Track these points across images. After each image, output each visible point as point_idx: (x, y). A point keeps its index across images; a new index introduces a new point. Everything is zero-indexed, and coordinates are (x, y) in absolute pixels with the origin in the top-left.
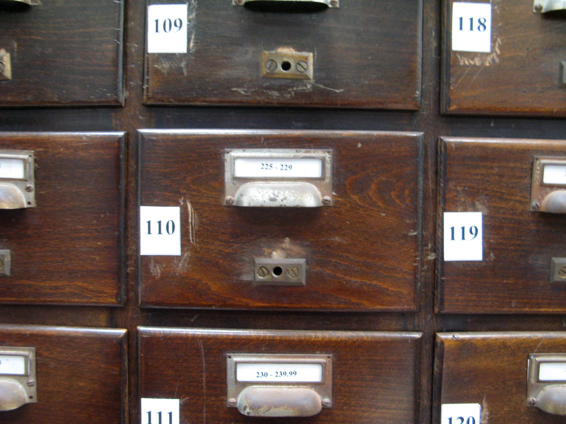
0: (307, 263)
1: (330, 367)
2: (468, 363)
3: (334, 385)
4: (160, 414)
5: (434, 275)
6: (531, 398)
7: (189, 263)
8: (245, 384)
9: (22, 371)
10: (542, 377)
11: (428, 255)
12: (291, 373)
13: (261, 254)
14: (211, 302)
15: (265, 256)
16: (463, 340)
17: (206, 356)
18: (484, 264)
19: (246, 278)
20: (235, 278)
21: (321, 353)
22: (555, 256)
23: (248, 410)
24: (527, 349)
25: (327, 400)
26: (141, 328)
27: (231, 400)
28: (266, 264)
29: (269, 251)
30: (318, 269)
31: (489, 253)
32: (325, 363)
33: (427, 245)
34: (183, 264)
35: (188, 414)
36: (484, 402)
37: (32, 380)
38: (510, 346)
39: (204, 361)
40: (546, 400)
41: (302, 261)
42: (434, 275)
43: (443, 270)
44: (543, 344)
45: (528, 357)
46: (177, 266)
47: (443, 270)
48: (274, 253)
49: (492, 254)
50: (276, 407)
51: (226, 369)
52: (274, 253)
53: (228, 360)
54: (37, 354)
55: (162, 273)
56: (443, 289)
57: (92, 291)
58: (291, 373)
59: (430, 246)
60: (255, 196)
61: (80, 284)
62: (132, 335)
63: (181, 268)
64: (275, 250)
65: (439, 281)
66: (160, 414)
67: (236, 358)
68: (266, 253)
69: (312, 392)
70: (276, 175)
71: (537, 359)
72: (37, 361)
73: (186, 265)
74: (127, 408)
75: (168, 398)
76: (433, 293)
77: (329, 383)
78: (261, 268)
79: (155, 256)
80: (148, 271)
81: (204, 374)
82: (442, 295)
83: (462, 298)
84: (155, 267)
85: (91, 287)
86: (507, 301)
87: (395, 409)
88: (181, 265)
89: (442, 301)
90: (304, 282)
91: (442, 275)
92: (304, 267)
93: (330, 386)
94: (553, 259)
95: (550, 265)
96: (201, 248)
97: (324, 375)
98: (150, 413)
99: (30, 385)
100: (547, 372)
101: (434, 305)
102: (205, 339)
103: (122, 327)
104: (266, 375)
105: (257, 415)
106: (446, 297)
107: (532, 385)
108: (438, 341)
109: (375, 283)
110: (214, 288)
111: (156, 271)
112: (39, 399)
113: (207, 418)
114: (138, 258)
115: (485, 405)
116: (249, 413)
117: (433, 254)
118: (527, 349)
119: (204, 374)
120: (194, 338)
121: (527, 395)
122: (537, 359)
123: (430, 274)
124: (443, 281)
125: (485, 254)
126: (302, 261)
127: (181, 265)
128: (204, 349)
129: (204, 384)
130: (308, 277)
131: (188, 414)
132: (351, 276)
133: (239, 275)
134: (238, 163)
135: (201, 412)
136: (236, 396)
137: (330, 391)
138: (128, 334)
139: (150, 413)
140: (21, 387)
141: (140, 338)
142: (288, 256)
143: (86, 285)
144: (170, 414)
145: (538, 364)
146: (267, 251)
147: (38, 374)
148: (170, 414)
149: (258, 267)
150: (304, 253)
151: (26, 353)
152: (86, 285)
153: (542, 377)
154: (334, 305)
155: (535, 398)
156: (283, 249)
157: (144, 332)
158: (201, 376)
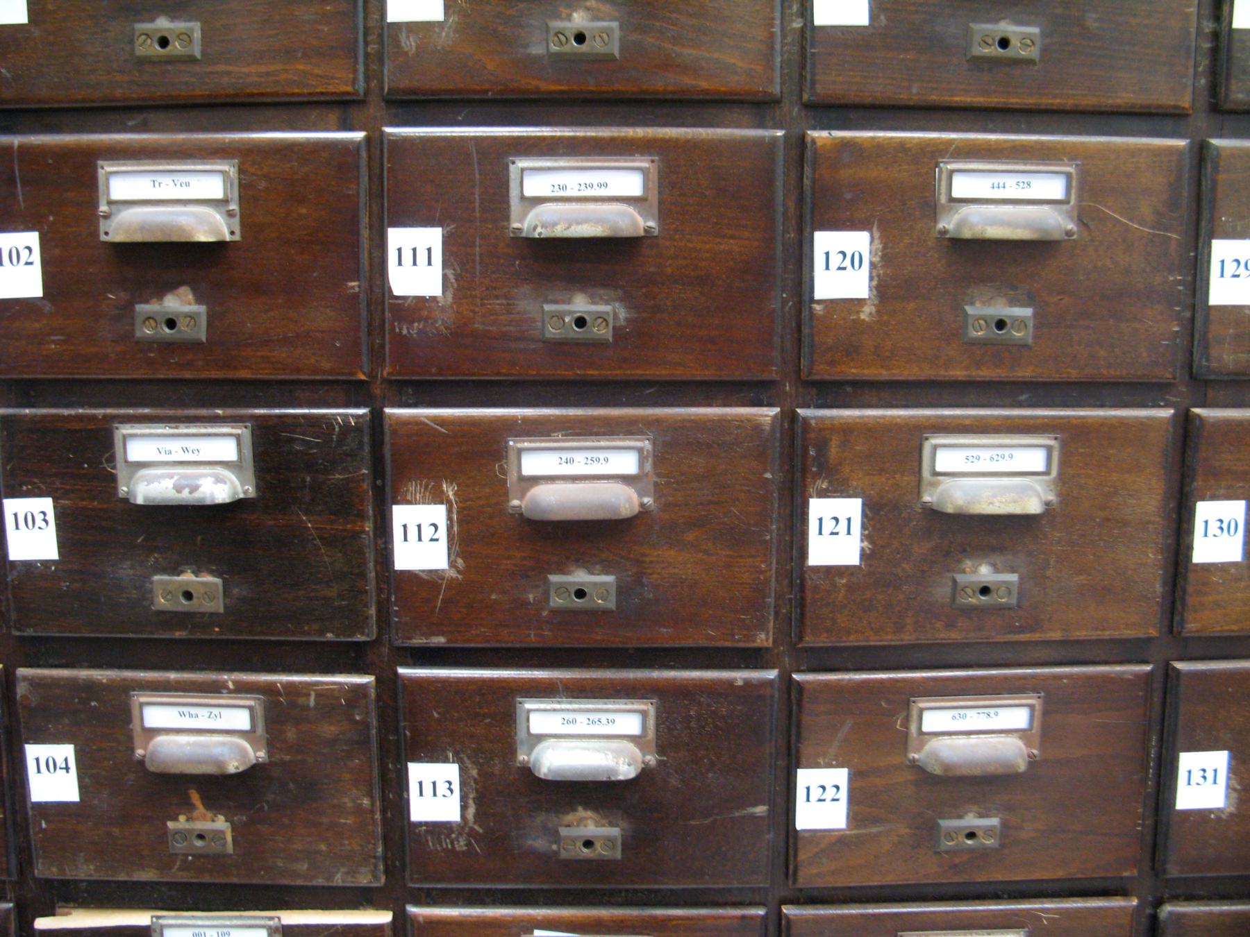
0: (621, 27)
1: (654, 175)
2: (851, 172)
3: (661, 202)
4: (414, 250)
5: (803, 48)
6: (941, 225)
7: (456, 31)
8: (535, 480)
9: (219, 195)
10: (956, 193)
11: (792, 21)
12: (600, 185)
13: (558, 16)
14: (486, 86)
15: (562, 19)
16: (843, 139)
17: (479, 164)
18: (872, 31)
19: (537, 50)
20: (521, 50)
21: (642, 155)
22: (974, 21)
23: (539, 230)
24: (920, 431)
25: (651, 224)
26: (388, 130)
27: (522, 757)
28: (565, 28)
29: (568, 11)
30: (635, 37)
31: (878, 16)
32: (648, 169)
33: (790, 7)
34: (448, 33)
35: (455, 249)
36: (875, 229)
37: (234, 206)
38: (910, 149)
39: (477, 172)
40: (935, 756)
41: (615, 25)
42: (803, 48)
43: (813, 37)
44: (957, 148)
45: (937, 165)
46: (439, 37)
47: (813, 37)
48: (575, 15)
49: (882, 17)
50: (578, 223)
51: (508, 181)
52: (575, 15)
53: (512, 167)
54: (241, 171)
55: (418, 47)
56: (814, 65)
57: (318, 76)
58: (600, 185)
59: (795, 8)
60: (551, 499)
61: (301, 67)
62: (375, 142)
63: (444, 39)
64: (575, 10)
65: (808, 55)
66: (414, 250)
67: (523, 163)
68: (564, 15)
69: (630, 210)
70: (581, 191)
71: (949, 167)
72: (240, 180)
73: (452, 35)
74: (366, 246)
75: (425, 226)
76: (801, 75)
77: (654, 198)
78: (556, 34)
79: (407, 23)
80: (397, 44)
81: (477, 191)
82: (813, 74)
83: (840, 79)
84: (408, 37)
85: (316, 71)
86: (907, 84)
87: (748, 239)
88: (444, 34)
89: (813, 83)
90: (617, 54)
91: (812, 46)
92: (617, 34)
93: (656, 203)
94: (971, 25)
95: (968, 33)
96: (472, 10)
97: (641, 464)
98: (400, 250)
99: (230, 214)
100: (963, 186)
101: (801, 91)
102: (478, 140)
103: (361, 129)
104: (564, 188)
105: (552, 235)
106: (818, 78)
107: (943, 206)
108: (808, 139)
109: (716, 55)
110: (490, 66)
111: (409, 43)
112: (243, 236)
113: (481, 255)
114: (382, 28)
115: (877, 235)
116: (540, 234)
117: (800, 20)
118: (936, 153)
119: (477, 191)
120: (463, 140)
121: (935, 221)
122: (949, 167)
123: (796, 49)
124: (813, 54)
125: (873, 16)
126: (615, 25)
127: (444, 34)
128: (478, 152)
129: (477, 205)
130: (622, 49)
131: (455, 249)
132: (683, 46)
133: (526, 46)
134: (533, 717)
135: (473, 245)
136: (521, 220)
137: (656, 211)
138: (368, 140)
139: (400, 250)
140: (218, 217)
141: (386, 142)
142: (596, 18)
143: (309, 68)
144: (429, 250)
145: (921, 711)
146: (564, 12)
147: (242, 199)
148: (429, 250)
149: (552, 32)
150: (616, 14)
151: (226, 168)
152: (309, 68)
153: (926, 728)
154: (662, 83)
155: (948, 223)
156: (588, 9)
157: (390, 134)
158: (473, 194)
